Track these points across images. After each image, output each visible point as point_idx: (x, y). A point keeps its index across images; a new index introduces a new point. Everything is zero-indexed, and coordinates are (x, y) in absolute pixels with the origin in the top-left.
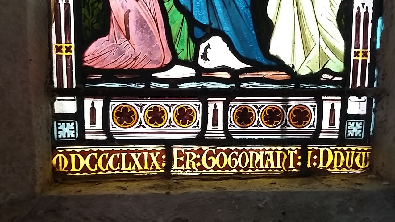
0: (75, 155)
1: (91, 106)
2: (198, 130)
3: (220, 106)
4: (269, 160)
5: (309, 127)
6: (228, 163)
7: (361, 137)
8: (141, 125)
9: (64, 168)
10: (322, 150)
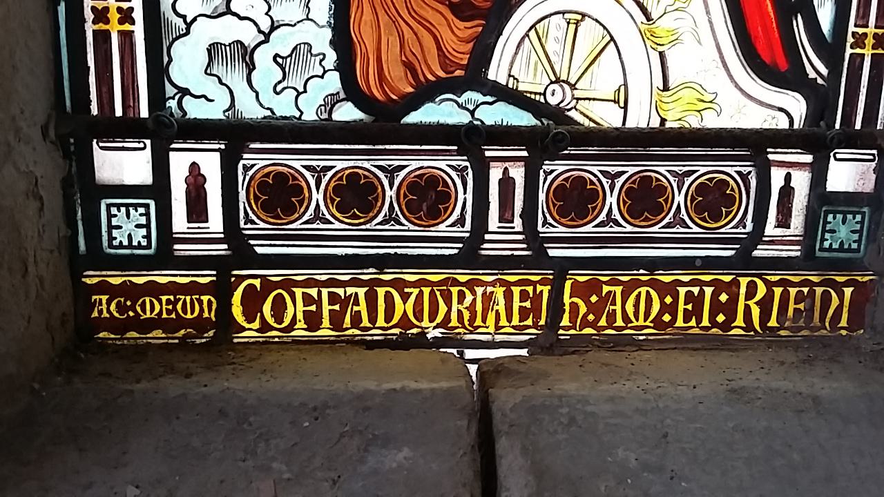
0: (387, 292)
1: (783, 184)
2: (465, 231)
3: (518, 173)
4: (356, 308)
5: (737, 224)
6: (405, 311)
7: (858, 250)
8: (610, 220)
9: (651, 318)
10: (744, 281)
